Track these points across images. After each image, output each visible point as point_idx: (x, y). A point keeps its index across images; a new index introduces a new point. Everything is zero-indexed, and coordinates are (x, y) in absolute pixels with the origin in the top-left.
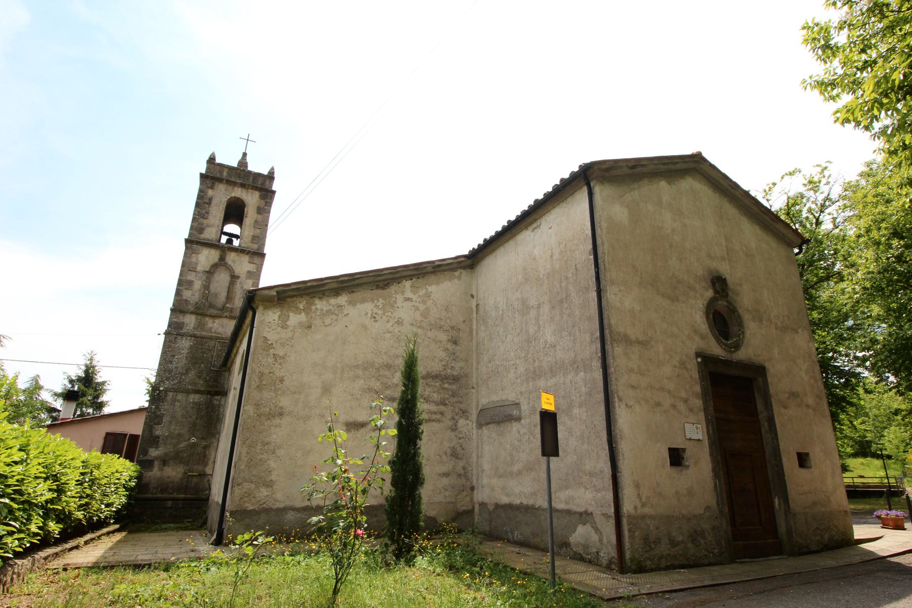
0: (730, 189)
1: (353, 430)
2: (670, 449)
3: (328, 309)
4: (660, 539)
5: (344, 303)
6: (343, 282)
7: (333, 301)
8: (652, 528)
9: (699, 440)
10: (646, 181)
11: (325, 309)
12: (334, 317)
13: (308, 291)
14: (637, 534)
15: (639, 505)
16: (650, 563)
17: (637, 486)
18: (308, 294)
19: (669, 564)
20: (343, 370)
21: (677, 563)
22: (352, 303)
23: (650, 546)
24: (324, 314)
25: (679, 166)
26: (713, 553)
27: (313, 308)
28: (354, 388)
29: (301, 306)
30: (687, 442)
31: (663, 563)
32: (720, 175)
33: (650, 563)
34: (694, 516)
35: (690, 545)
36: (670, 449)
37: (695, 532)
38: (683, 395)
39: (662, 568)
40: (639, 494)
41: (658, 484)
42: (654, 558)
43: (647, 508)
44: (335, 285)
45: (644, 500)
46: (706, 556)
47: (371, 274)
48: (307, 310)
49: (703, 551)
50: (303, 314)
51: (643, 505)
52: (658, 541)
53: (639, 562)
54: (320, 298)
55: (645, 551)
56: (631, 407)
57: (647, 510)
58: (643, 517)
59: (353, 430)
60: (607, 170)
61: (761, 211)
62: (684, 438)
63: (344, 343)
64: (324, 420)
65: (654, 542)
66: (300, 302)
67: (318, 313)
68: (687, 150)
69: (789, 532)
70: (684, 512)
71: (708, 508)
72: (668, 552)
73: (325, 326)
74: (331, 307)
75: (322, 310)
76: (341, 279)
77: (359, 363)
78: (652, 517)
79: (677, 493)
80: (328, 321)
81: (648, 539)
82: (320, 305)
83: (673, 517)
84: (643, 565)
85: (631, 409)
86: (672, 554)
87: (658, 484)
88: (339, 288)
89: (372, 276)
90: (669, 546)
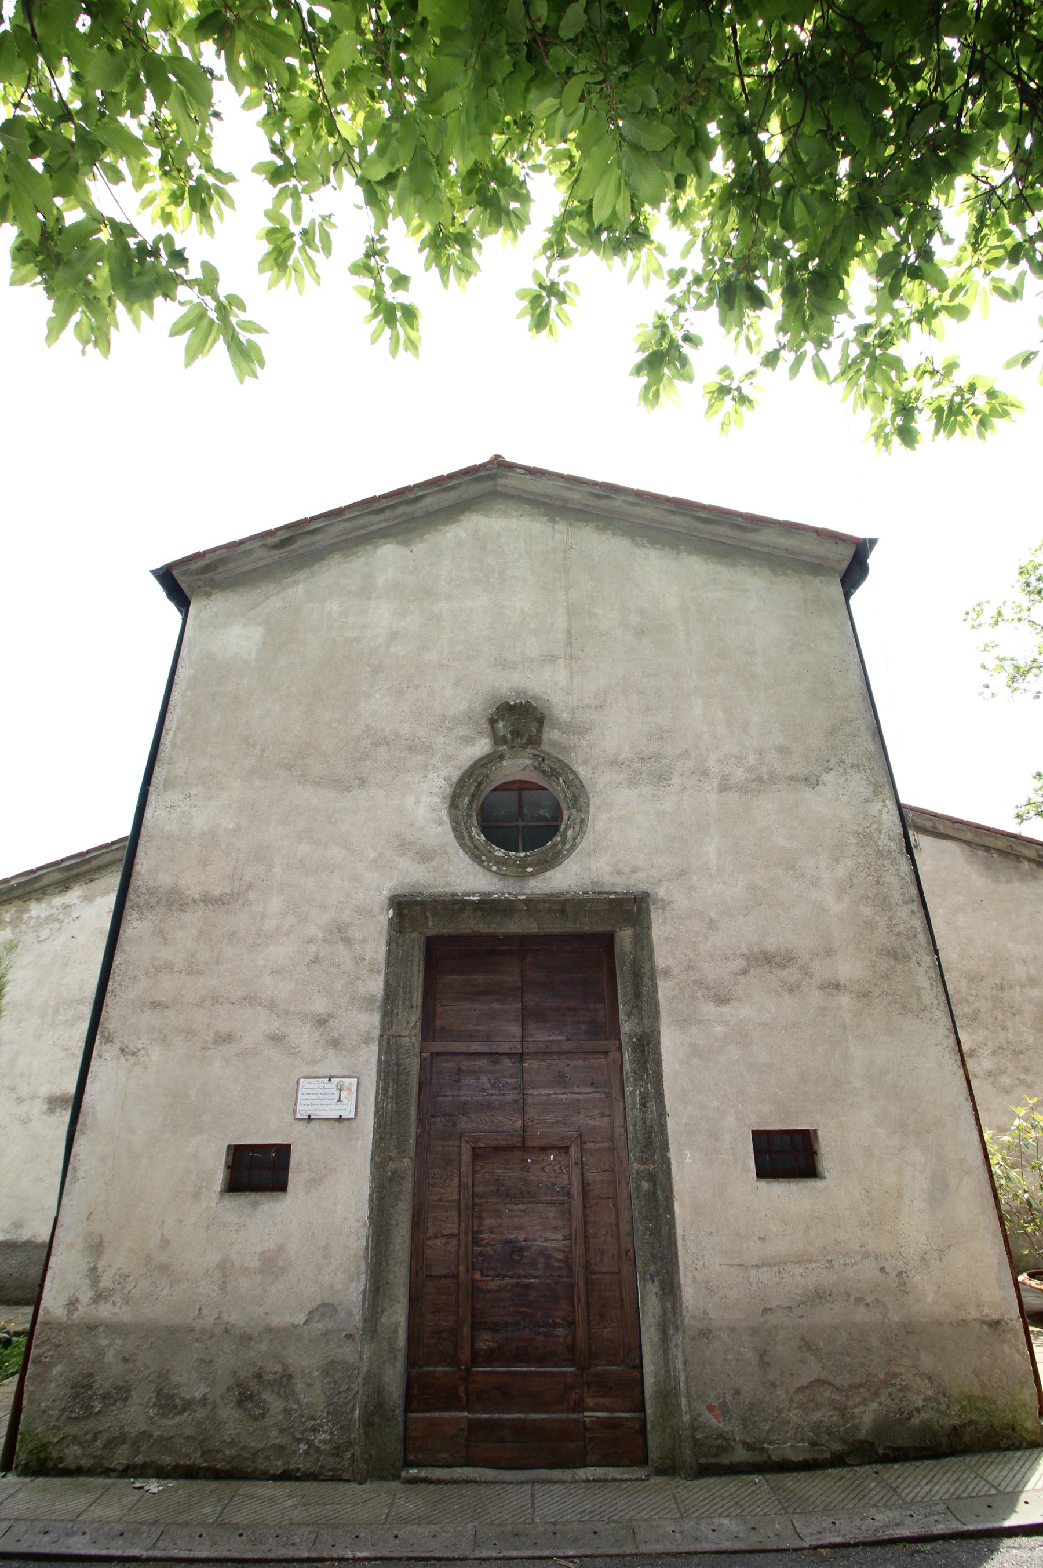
0: (591, 501)
1: (58, 1110)
2: (284, 1151)
3: (48, 914)
4: (128, 1390)
5: (76, 901)
6: (69, 868)
7: (58, 901)
8: (110, 1356)
9: (340, 1119)
10: (337, 557)
11: (43, 915)
12: (56, 925)
13: (16, 893)
14: (56, 1370)
15: (86, 1296)
16: (79, 1452)
17: (96, 1247)
18: (19, 898)
19: (139, 1459)
20: (57, 1009)
21: (167, 1460)
22: (88, 899)
23: (87, 1407)
24: (40, 924)
25: (430, 502)
26: (310, 1444)
27: (26, 916)
28: (70, 1037)
29: (7, 917)
30: (301, 1126)
31: (121, 1457)
32: (560, 483)
33: (79, 1452)
34: (269, 1330)
35: (228, 1413)
36: (284, 1151)
37: (259, 1376)
38: (320, 1005)
39: (114, 1470)
40: (95, 1268)
41: (165, 1242)
42: (95, 1439)
43: (109, 1305)
44: (58, 876)
45: (106, 1282)
46: (281, 1448)
47: (114, 847)
48: (14, 923)
49: (274, 1433)
50: (9, 930)
51: (99, 1297)
52: (122, 1393)
53: (44, 1446)
54: (39, 900)
55: (69, 1418)
56: (134, 1054)
57: (105, 1311)
58: (91, 1328)
59: (58, 1110)
60: (207, 568)
61: (698, 519)
62: (289, 1118)
63: (66, 965)
64: (15, 1096)
65: (105, 1397)
66: (7, 911)
67: (32, 924)
68: (481, 457)
69: (668, 1394)
70: (234, 1317)
71: (325, 1309)
72: (144, 1427)
73: (40, 942)
74: (54, 911)
75: (38, 917)
76: (64, 864)
77: (86, 994)
78: (115, 1329)
79: (223, 1266)
80: (44, 933)
81: (89, 1386)
82: (37, 909)
83: (192, 1330)
84: (55, 1454)
85: (133, 1059)
86: (156, 1434)
87: (165, 1242)
88: (68, 878)
89: (117, 849)
90: (152, 1412)
